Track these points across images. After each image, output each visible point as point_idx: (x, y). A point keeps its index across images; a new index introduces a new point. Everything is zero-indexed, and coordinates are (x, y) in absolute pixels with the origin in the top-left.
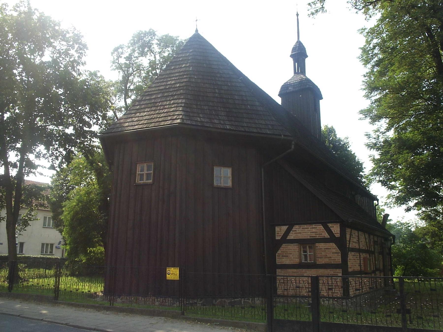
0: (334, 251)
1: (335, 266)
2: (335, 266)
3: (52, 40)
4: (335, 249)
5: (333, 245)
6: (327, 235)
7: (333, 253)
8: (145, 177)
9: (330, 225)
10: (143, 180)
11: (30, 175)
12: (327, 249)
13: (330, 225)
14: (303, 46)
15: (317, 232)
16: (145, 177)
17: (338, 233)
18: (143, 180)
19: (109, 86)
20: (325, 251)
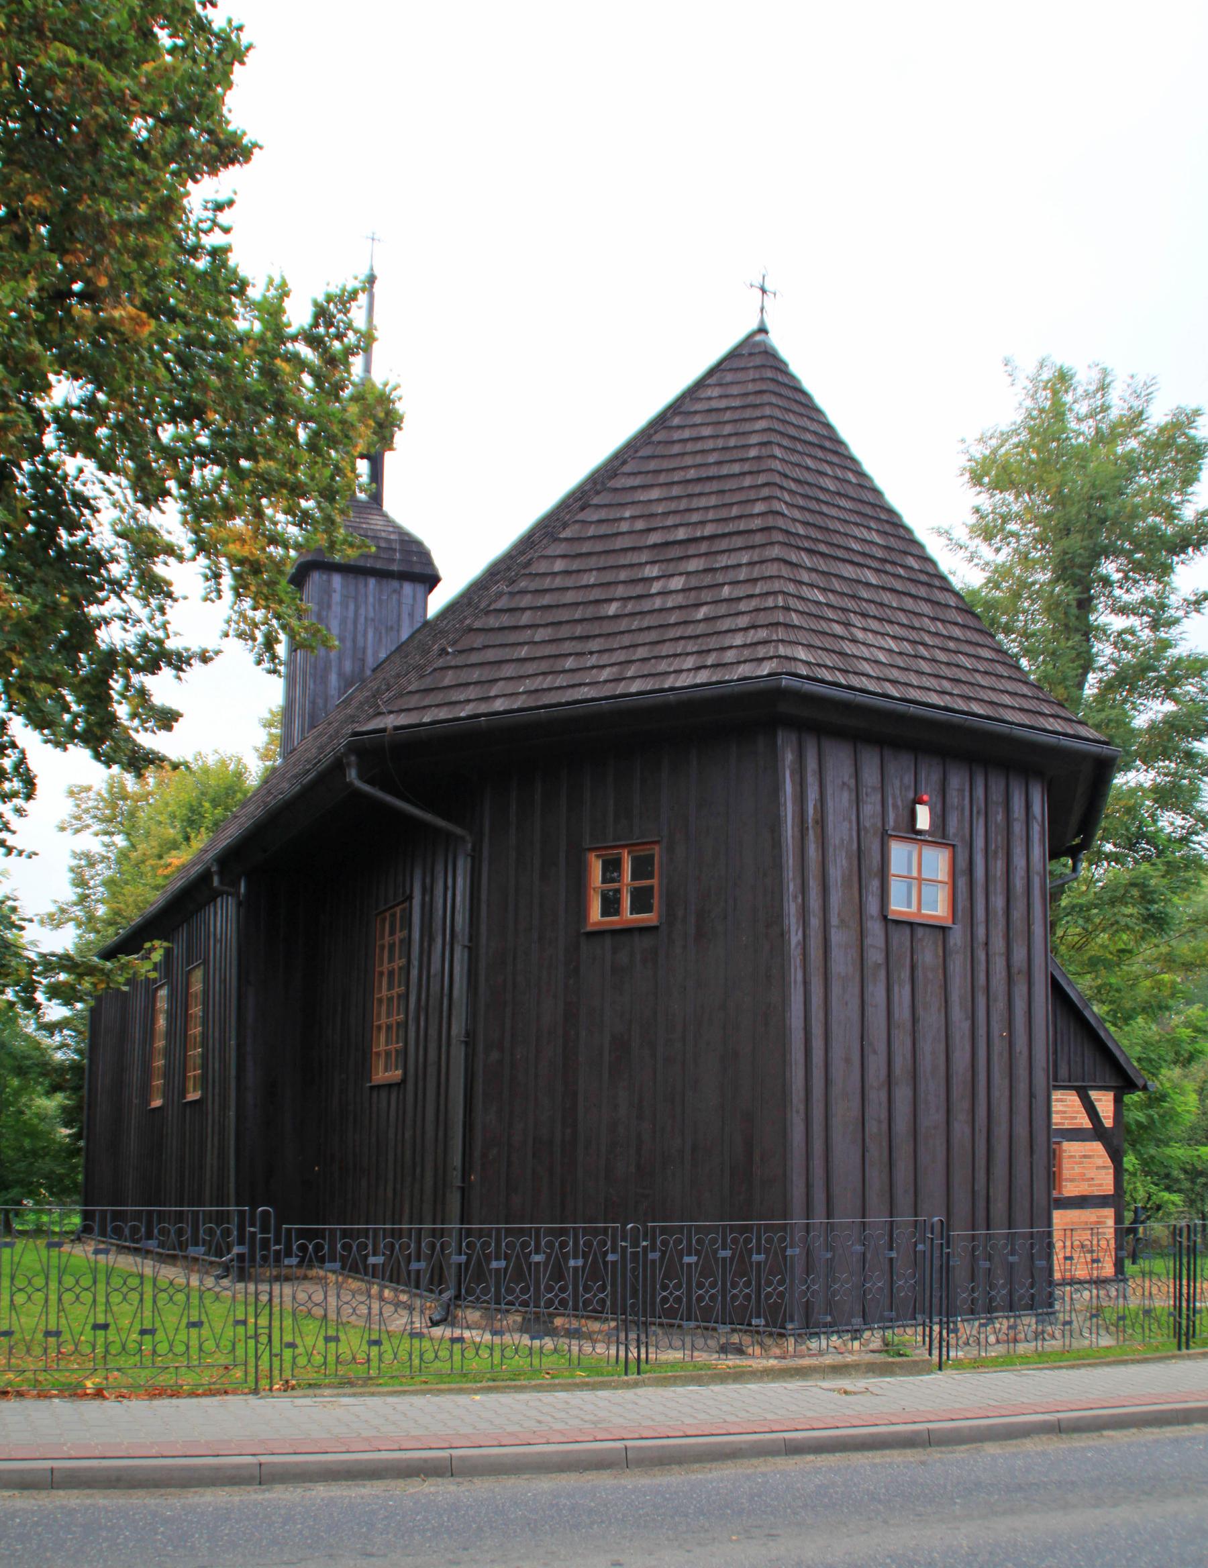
0: (1100, 1162)
1: (1100, 1201)
2: (1100, 1201)
3: (138, 10)
4: (1101, 1156)
5: (1097, 1147)
6: (1086, 1123)
7: (1098, 1168)
8: (627, 902)
9: (1094, 1095)
10: (617, 912)
11: (70, 802)
12: (1084, 1157)
13: (1094, 1095)
14: (419, 544)
15: (1065, 1112)
16: (627, 902)
17: (1057, 1100)
18: (617, 912)
19: (1055, 393)
20: (1081, 1163)
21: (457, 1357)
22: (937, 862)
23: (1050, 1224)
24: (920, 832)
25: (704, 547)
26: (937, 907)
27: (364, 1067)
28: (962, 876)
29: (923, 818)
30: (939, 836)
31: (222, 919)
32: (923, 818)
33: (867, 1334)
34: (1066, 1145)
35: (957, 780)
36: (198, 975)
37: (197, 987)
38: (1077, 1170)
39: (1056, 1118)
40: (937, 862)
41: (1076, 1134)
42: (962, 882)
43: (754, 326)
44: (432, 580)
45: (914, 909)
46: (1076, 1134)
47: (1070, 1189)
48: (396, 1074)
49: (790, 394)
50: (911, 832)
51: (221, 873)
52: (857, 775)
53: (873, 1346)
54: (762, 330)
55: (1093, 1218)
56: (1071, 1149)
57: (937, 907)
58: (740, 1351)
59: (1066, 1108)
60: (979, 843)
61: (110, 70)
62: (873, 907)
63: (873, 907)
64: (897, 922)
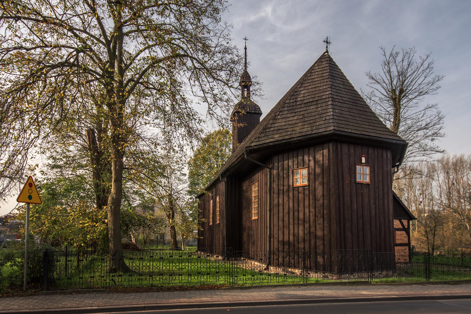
0: (405, 236)
5: (404, 232)
6: (401, 227)
9: (403, 221)
13: (403, 221)
21: (199, 279)
22: (359, 179)
23: (394, 251)
24: (363, 163)
25: (315, 103)
26: (367, 180)
27: (251, 217)
28: (373, 174)
29: (364, 160)
30: (367, 164)
31: (222, 186)
32: (364, 160)
33: (354, 274)
34: (397, 232)
35: (371, 151)
36: (218, 197)
37: (218, 199)
38: (399, 237)
39: (395, 226)
40: (359, 179)
41: (399, 230)
42: (372, 174)
43: (325, 51)
44: (260, 114)
45: (362, 180)
46: (399, 230)
47: (398, 242)
48: (256, 218)
49: (333, 66)
50: (361, 164)
51: (221, 177)
52: (349, 150)
53: (356, 277)
54: (327, 52)
55: (404, 249)
56: (398, 233)
57: (367, 180)
58: (327, 277)
59: (397, 224)
60: (376, 165)
61: (279, 294)
62: (353, 181)
63: (353, 181)
64: (358, 183)
